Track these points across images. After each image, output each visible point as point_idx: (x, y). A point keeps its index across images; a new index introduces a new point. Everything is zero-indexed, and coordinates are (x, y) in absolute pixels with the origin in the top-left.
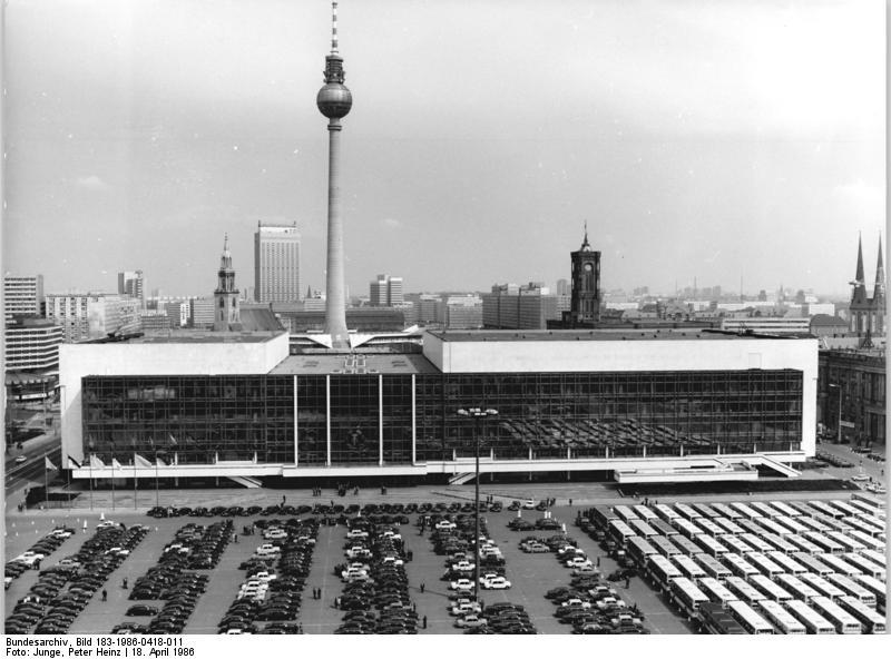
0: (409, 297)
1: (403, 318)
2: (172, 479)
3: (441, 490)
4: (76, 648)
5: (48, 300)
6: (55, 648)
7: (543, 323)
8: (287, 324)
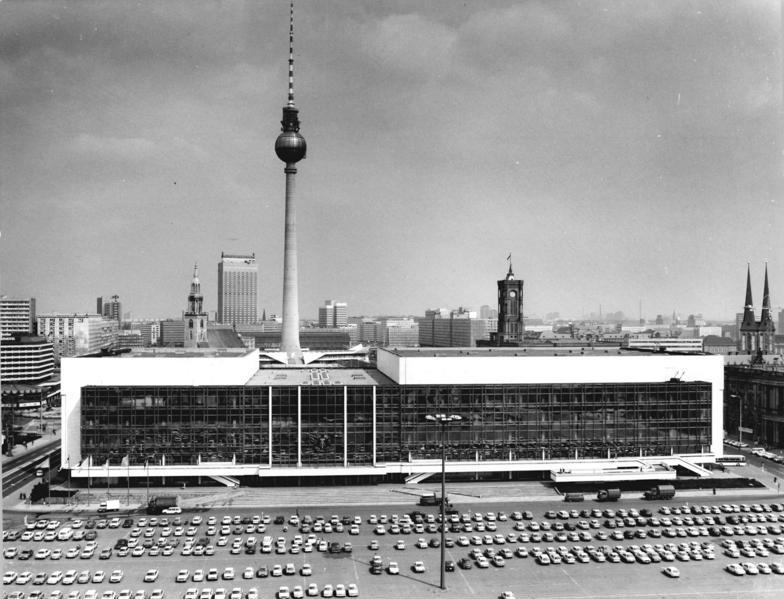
0: (353, 319)
1: (349, 339)
2: (159, 479)
3: (399, 488)
5: (39, 320)
7: (473, 343)
8: (251, 342)
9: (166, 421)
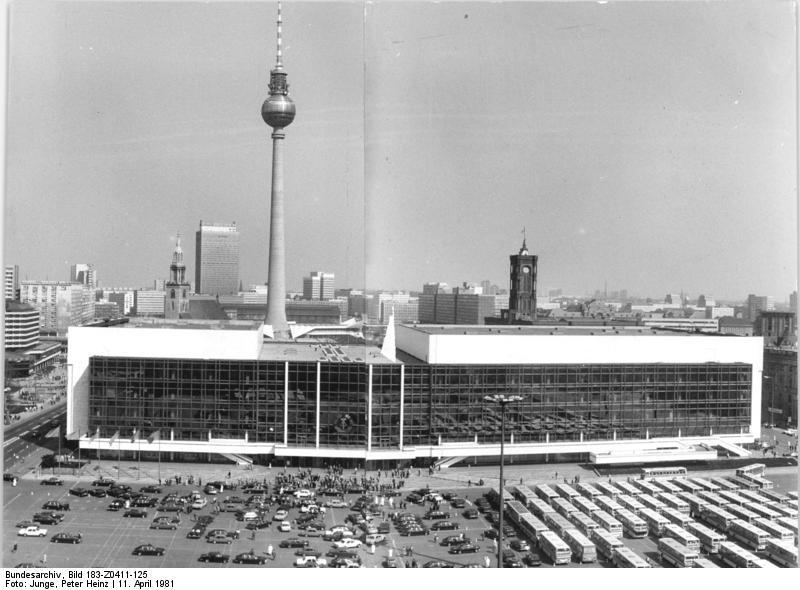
4: (69, 580)
5: (22, 287)
6: (50, 580)
9: (175, 394)
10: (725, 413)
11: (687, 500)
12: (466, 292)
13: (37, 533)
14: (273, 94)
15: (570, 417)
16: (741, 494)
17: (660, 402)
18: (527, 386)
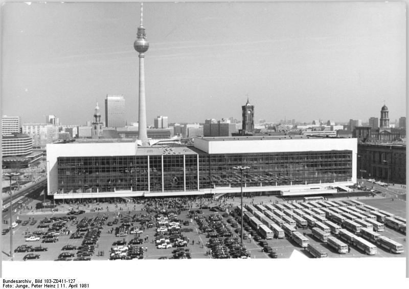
4: (35, 284)
6: (25, 284)
9: (98, 172)
10: (340, 173)
11: (324, 211)
12: (224, 123)
13: (35, 239)
14: (139, 37)
15: (271, 175)
16: (348, 208)
17: (311, 169)
18: (251, 162)
